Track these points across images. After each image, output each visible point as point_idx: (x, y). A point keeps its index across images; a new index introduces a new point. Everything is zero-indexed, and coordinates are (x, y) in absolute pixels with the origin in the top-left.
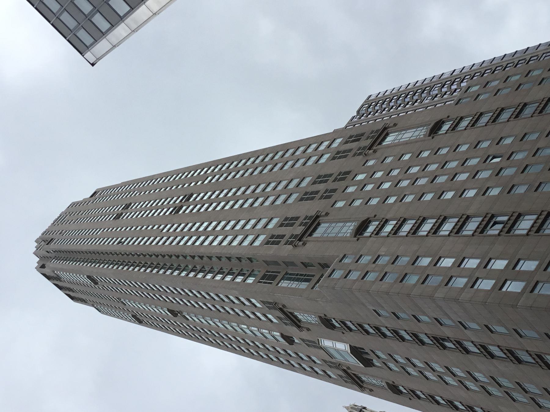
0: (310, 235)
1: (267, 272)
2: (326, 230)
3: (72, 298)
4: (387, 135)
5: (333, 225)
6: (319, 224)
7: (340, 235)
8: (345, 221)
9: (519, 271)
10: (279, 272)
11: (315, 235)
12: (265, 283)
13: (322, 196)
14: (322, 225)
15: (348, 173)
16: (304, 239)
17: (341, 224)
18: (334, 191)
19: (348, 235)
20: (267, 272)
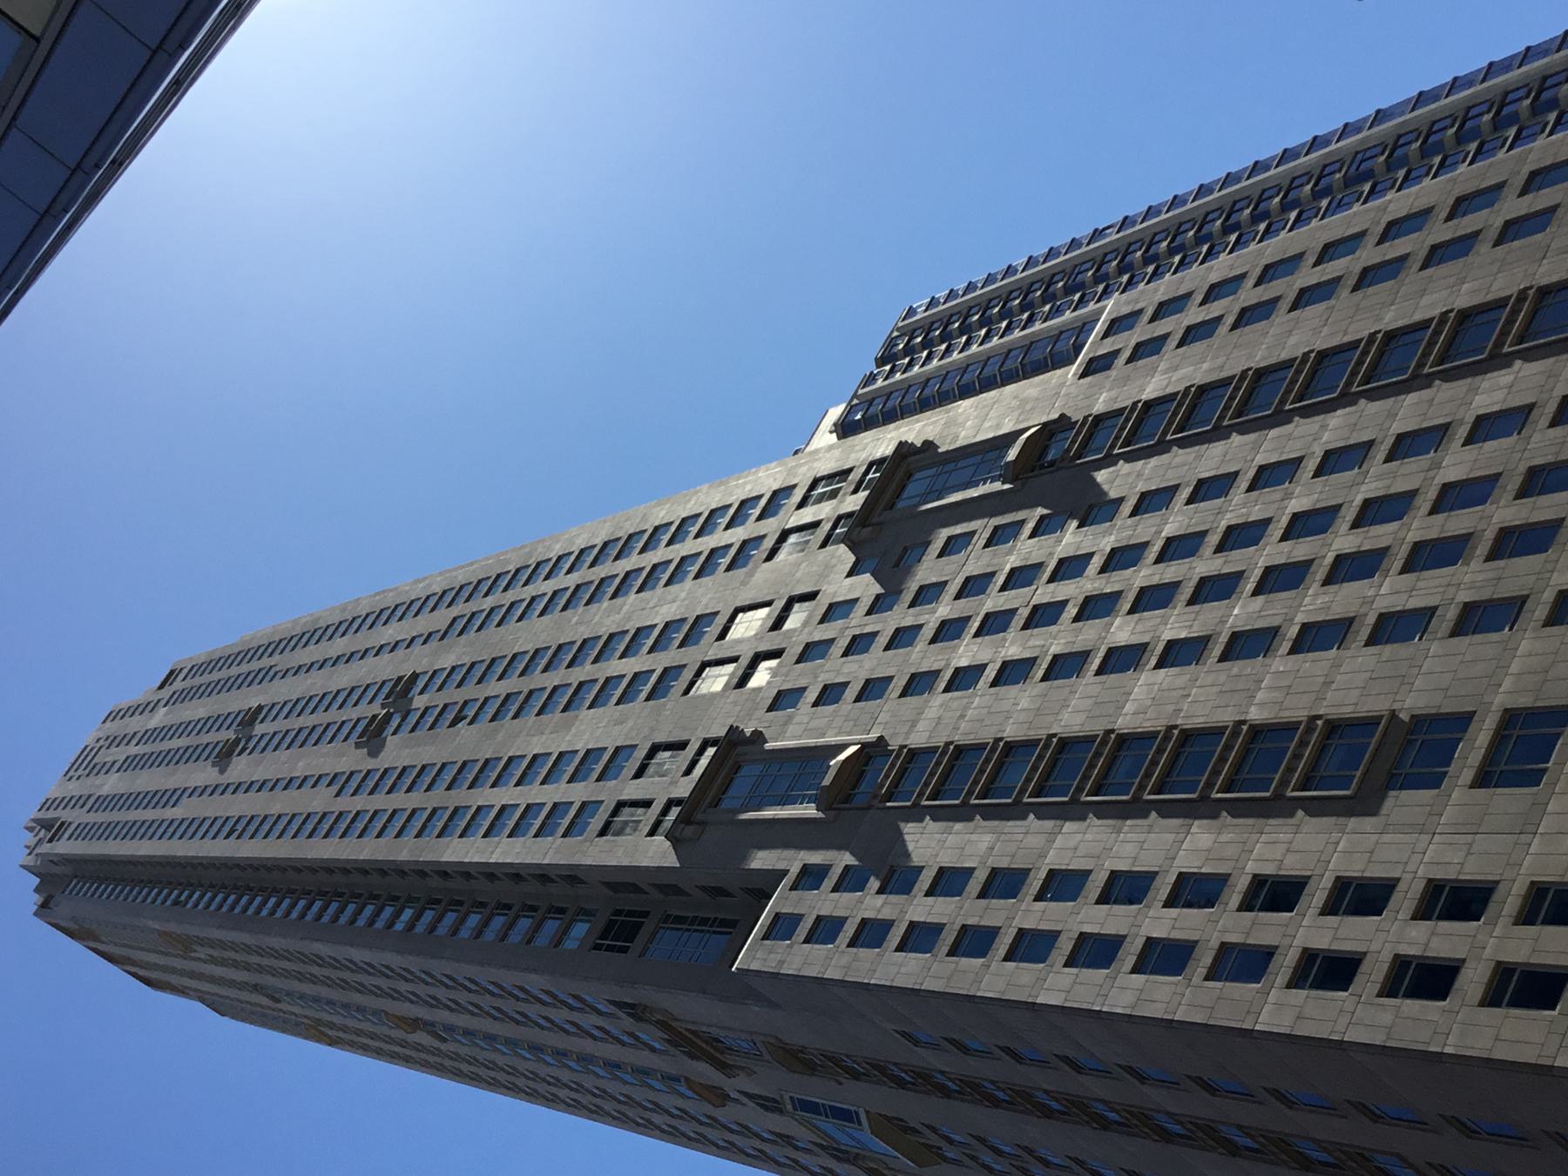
0: (891, 506)
1: (618, 913)
3: (147, 982)
6: (909, 476)
11: (900, 505)
12: (610, 948)
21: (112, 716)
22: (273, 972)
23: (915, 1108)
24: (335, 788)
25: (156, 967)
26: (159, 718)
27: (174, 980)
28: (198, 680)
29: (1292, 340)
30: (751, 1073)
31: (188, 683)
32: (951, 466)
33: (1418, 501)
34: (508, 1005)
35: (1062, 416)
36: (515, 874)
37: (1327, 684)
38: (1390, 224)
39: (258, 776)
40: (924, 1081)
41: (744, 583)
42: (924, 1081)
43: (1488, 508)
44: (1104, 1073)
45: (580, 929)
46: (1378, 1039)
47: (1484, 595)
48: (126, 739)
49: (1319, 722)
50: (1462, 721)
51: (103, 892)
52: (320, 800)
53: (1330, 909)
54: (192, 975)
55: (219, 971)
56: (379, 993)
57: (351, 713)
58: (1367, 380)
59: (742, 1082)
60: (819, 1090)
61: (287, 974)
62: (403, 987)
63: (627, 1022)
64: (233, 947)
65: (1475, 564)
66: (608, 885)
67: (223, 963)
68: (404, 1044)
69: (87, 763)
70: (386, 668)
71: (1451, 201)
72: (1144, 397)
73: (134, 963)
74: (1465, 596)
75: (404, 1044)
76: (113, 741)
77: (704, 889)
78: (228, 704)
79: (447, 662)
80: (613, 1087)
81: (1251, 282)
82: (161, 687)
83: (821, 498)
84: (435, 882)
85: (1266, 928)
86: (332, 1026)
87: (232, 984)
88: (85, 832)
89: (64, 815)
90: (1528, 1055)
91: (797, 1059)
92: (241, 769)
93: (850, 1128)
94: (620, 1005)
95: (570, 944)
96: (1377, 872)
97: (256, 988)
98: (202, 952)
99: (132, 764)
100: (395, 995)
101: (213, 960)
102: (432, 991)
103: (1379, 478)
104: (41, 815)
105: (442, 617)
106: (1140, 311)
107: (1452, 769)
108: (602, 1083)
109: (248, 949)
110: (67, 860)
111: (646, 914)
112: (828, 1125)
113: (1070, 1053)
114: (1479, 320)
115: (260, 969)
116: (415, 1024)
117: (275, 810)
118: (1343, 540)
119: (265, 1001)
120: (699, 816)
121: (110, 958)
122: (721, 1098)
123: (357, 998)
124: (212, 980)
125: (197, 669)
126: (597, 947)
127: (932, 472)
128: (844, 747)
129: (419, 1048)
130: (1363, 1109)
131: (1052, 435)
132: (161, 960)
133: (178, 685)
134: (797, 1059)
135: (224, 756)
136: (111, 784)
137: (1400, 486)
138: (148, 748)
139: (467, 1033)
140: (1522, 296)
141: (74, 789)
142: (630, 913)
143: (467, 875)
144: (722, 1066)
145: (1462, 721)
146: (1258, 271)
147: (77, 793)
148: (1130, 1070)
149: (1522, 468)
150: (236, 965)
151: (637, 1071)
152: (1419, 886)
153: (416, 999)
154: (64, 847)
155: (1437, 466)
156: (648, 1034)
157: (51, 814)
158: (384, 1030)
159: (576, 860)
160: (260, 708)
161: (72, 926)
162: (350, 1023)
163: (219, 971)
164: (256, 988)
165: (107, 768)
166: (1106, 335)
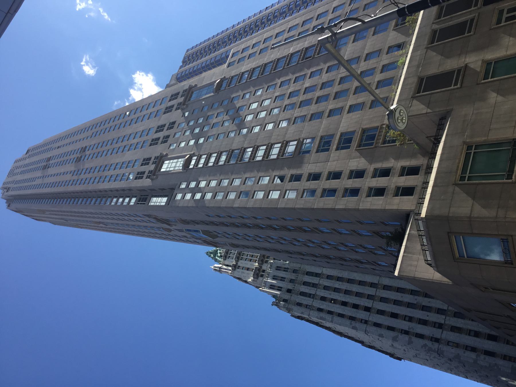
0: (189, 100)
1: (141, 196)
2: (168, 166)
3: (36, 220)
4: (163, 163)
5: (172, 161)
6: (192, 93)
7: (176, 168)
8: (178, 158)
9: (276, 184)
10: (148, 196)
11: (192, 99)
12: (141, 204)
13: (168, 128)
14: (195, 93)
15: (174, 123)
16: (186, 103)
17: (176, 161)
18: (168, 137)
19: (181, 168)
20: (141, 196)
21: (16, 162)
22: (65, 215)
23: (211, 228)
24: (72, 174)
25: (38, 216)
26: (27, 161)
27: (43, 219)
28: (35, 152)
29: (272, 56)
30: (175, 225)
31: (32, 152)
32: (202, 90)
33: (301, 91)
34: (120, 217)
35: (225, 77)
36: (31, 195)
37: (233, 143)
38: (318, 15)
39: (53, 173)
40: (213, 223)
41: (159, 120)
42: (213, 223)
43: (315, 92)
44: (248, 218)
45: (134, 200)
46: (302, 207)
47: (315, 111)
48: (20, 167)
49: (384, 126)
50: (332, 136)
51: (26, 201)
52: (68, 177)
53: (290, 181)
54: (47, 217)
55: (52, 216)
56: (90, 217)
57: (72, 157)
58: (318, 54)
59: (174, 227)
60: (190, 227)
61: (68, 215)
62: (95, 216)
63: (148, 218)
64: (55, 211)
65: (313, 105)
66: (138, 190)
67: (53, 214)
68: (98, 227)
69: (11, 173)
70: (79, 146)
71: (302, 22)
72: (242, 71)
73: (32, 216)
74: (311, 112)
75: (98, 227)
76: (17, 168)
77: (160, 189)
78: (42, 157)
79: (93, 143)
80: (153, 231)
81: (315, 19)
82: (26, 154)
83: (173, 99)
84: (72, 194)
85: (333, 184)
86: (81, 225)
87: (56, 218)
88: (14, 189)
89: (9, 186)
90: (330, 206)
91: (185, 222)
92: (50, 171)
93: (198, 233)
94: (145, 215)
95: (132, 204)
96: (337, 170)
97: (62, 219)
98: (48, 213)
99: (22, 173)
100: (94, 218)
101: (50, 214)
102: (123, 217)
103: (293, 87)
104: (4, 186)
105: (90, 133)
106: (239, 51)
107: (331, 147)
108: (150, 231)
109: (58, 211)
110: (12, 196)
111: (148, 196)
112: (194, 234)
113: (229, 215)
114: (310, 49)
115: (62, 215)
116: (100, 223)
117: (58, 180)
118: (337, 88)
119: (104, 226)
120: (157, 174)
121: (27, 216)
122: (170, 230)
123: (86, 219)
124: (53, 218)
125: (34, 148)
126: (138, 204)
127: (198, 91)
128: (187, 155)
129: (101, 227)
130: (318, 220)
131: (223, 81)
132: (39, 215)
133: (30, 153)
134: (185, 222)
135: (45, 168)
136: (19, 177)
137: (297, 89)
138: (26, 169)
139: (112, 223)
140: (288, 55)
141: (10, 179)
142: (144, 196)
143: (106, 191)
144: (169, 225)
145: (332, 136)
146: (288, 29)
147: (11, 180)
148: (254, 217)
149: (321, 83)
150: (56, 215)
151: (151, 227)
152: (307, 174)
153: (98, 218)
154: (11, 193)
155: (304, 84)
156: (152, 220)
157: (6, 186)
158: (93, 225)
159: (130, 186)
160: (51, 157)
161: (16, 210)
162: (88, 224)
163: (52, 216)
164: (62, 219)
165: (17, 174)
166: (232, 57)
